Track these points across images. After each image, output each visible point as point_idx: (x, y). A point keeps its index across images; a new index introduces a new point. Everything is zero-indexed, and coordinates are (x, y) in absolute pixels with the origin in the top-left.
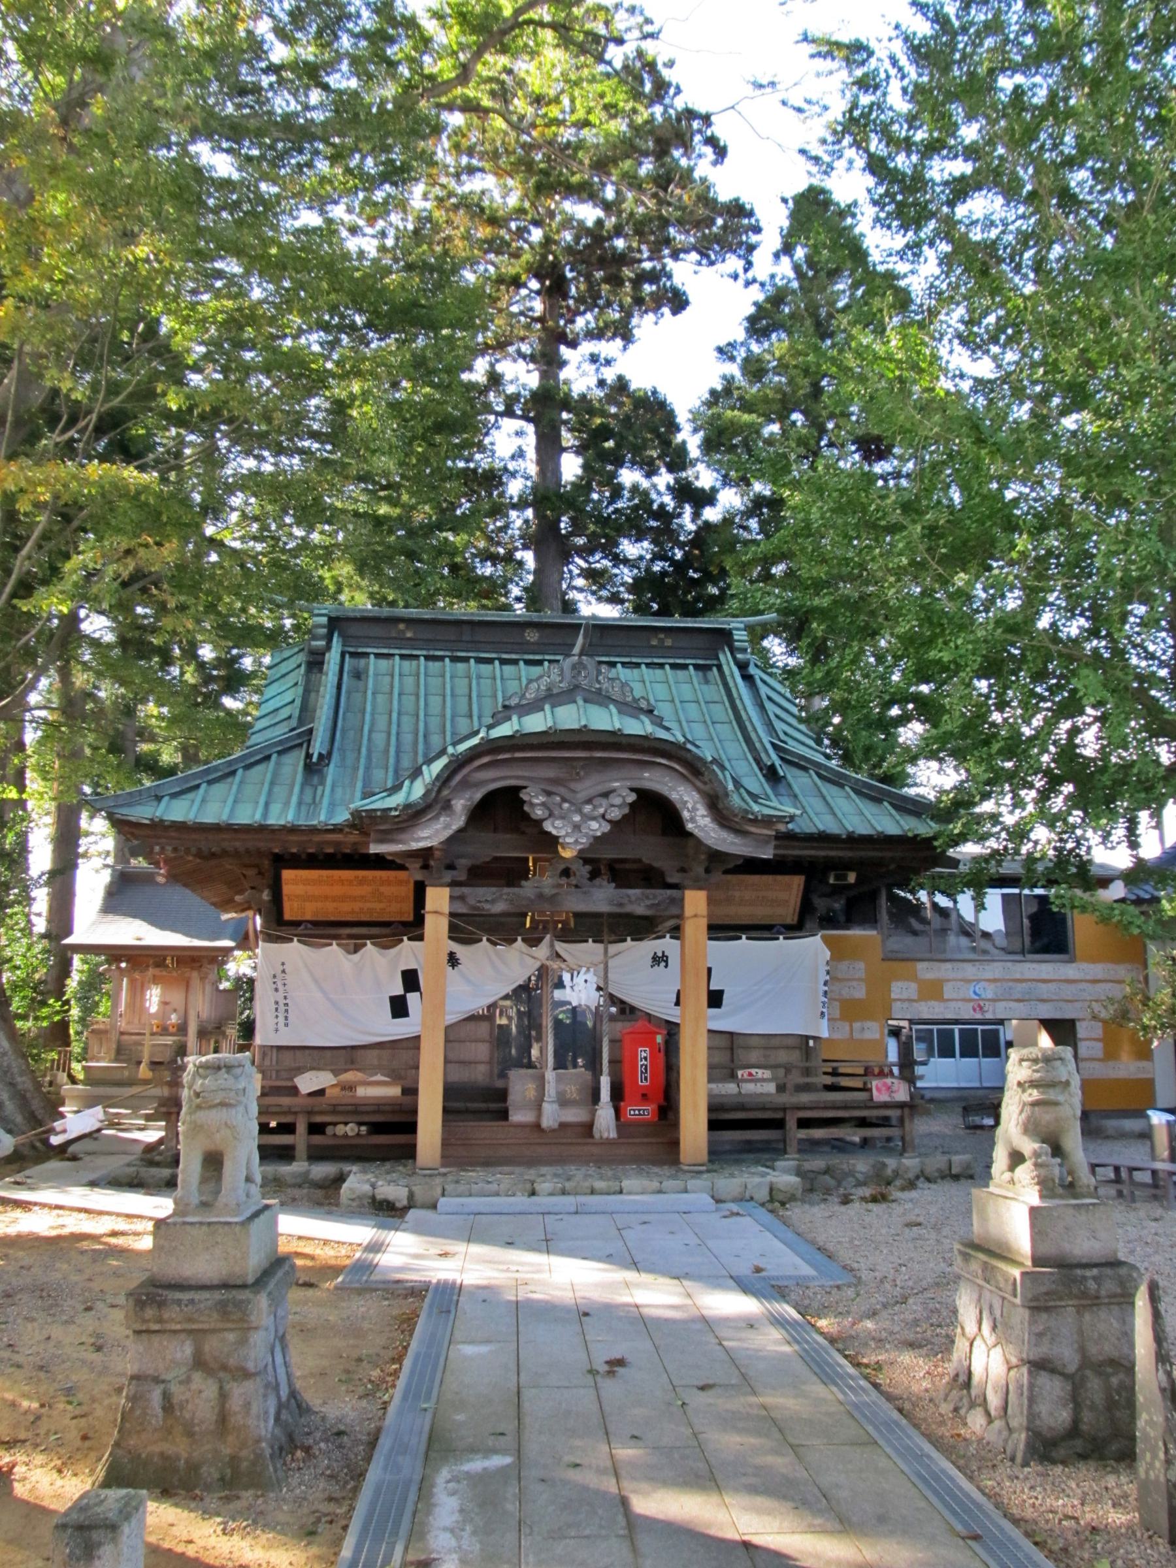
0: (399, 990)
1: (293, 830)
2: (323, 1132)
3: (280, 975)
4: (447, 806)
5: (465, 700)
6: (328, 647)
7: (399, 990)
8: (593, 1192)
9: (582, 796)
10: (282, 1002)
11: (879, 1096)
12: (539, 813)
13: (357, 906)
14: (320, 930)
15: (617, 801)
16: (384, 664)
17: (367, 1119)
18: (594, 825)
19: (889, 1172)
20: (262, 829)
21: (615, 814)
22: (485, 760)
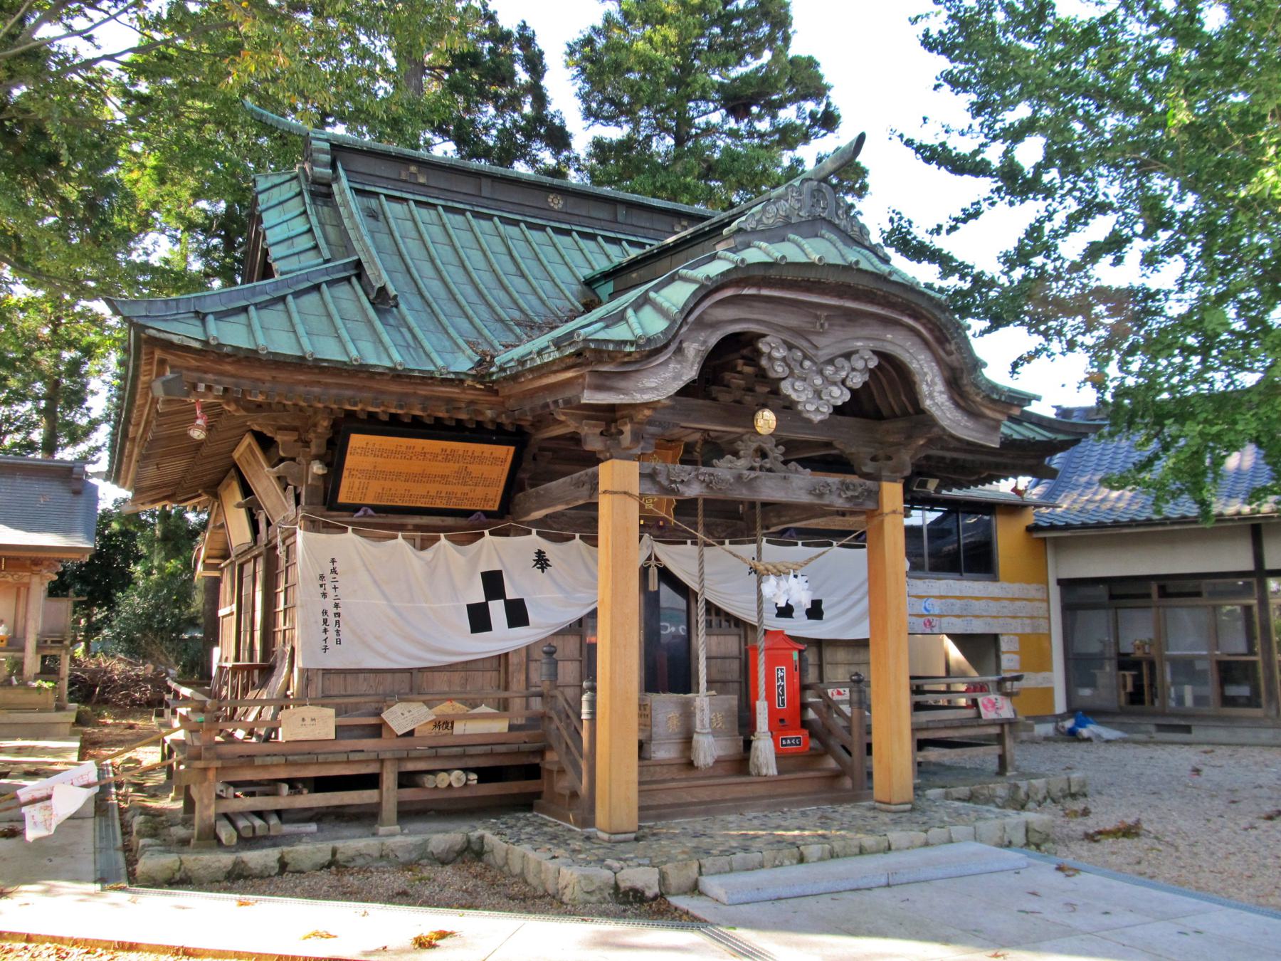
0: (478, 596)
2: (416, 785)
3: (329, 576)
6: (336, 178)
7: (478, 596)
8: (862, 851)
9: (824, 354)
10: (332, 611)
11: (988, 714)
12: (779, 370)
13: (433, 488)
14: (386, 518)
15: (860, 364)
17: (472, 763)
18: (836, 391)
19: (1022, 794)
20: (361, 371)
21: (857, 381)
22: (729, 293)
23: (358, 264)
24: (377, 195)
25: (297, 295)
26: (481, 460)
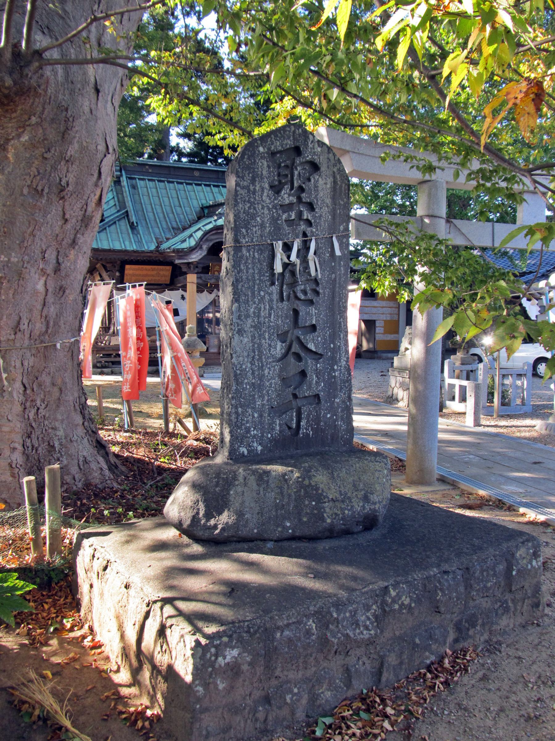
1: (134, 252)
4: (201, 248)
5: (176, 200)
6: (121, 175)
16: (142, 182)
20: (126, 252)
23: (127, 212)
24: (135, 179)
25: (109, 226)
26: (163, 270)
